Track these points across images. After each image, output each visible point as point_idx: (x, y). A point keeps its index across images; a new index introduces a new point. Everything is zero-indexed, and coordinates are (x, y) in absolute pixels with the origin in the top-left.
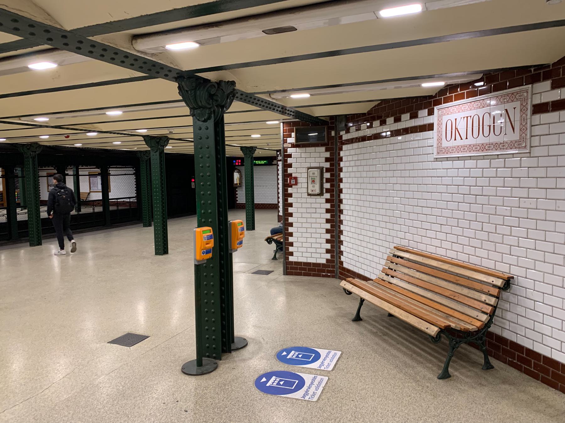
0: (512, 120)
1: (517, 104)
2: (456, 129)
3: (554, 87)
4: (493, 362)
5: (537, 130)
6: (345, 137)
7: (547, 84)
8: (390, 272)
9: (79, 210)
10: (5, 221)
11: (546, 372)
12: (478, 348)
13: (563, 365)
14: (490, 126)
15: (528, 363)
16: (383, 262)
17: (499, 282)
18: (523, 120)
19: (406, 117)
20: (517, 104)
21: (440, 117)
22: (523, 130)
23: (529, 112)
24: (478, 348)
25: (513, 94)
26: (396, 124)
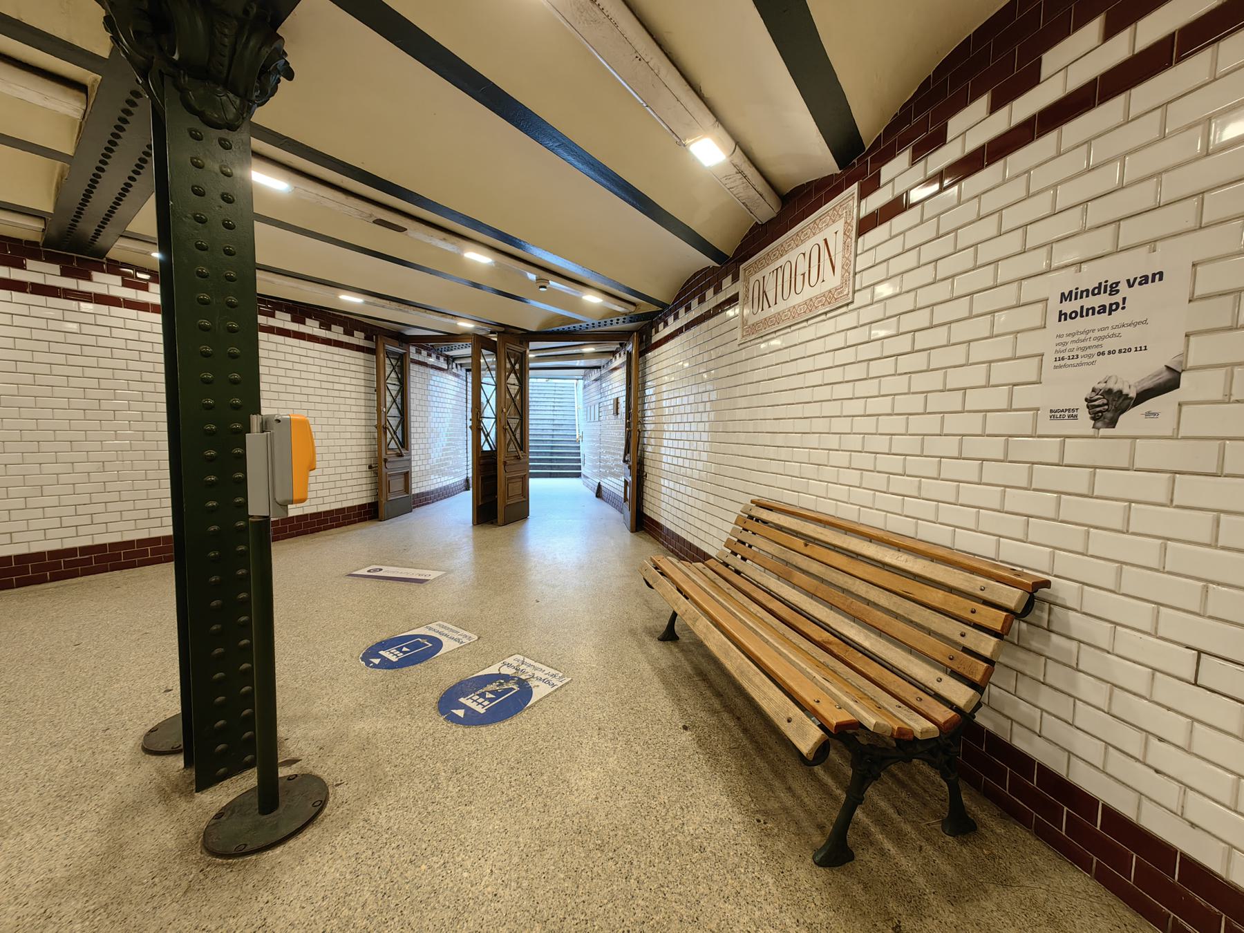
5: (862, 262)
6: (656, 338)
25: (797, 234)
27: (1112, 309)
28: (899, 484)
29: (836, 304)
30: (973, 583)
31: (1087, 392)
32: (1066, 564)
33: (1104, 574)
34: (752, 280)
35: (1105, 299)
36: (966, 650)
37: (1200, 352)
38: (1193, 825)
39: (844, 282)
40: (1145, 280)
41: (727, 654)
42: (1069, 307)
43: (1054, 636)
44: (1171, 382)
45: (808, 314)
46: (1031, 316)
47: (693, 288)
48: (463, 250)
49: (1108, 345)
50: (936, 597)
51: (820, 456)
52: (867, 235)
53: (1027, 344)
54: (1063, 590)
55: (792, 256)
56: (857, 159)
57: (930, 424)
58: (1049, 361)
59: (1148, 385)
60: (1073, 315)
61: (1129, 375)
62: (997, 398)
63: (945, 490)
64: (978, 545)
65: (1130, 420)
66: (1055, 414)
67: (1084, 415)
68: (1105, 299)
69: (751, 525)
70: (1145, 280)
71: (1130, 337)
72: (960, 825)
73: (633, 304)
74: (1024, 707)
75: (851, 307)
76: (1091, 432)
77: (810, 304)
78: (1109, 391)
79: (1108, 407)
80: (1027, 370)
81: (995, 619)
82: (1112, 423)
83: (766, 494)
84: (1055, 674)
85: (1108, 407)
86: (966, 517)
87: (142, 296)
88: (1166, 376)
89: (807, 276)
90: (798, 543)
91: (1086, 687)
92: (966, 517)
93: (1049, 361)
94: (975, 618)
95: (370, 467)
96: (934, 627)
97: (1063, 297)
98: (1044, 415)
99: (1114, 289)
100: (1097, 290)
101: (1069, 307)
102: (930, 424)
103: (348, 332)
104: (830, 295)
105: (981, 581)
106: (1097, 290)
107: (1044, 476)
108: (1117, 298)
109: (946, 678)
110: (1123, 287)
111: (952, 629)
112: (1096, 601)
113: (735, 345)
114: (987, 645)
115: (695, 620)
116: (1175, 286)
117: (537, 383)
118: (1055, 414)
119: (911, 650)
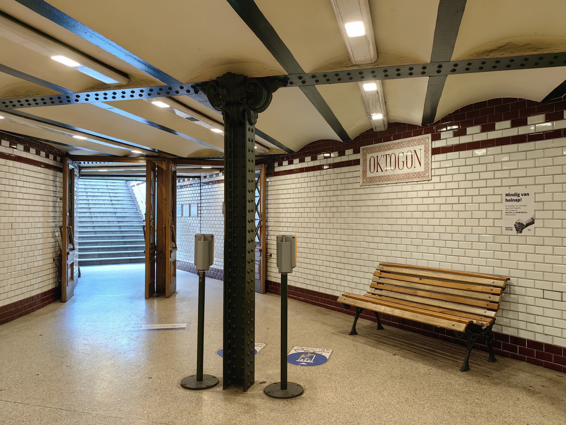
0: (419, 157)
1: (422, 147)
2: (378, 163)
3: (483, 131)
4: (497, 357)
5: (434, 165)
6: (277, 169)
7: (542, 117)
8: (380, 286)
9: (171, 111)
10: (374, 114)
11: (531, 353)
12: (481, 345)
13: (564, 349)
14: (403, 162)
15: (531, 353)
16: (371, 276)
17: (501, 283)
18: (426, 157)
19: (296, 161)
20: (422, 147)
21: (365, 155)
22: (426, 164)
23: (430, 152)
24: (481, 345)
25: (398, 143)
26: (340, 158)
27: (518, 201)
28: (456, 252)
29: (422, 178)
30: (490, 282)
31: (514, 223)
32: (513, 273)
33: (521, 274)
34: (369, 156)
35: (516, 198)
36: (491, 302)
37: (538, 215)
38: (546, 335)
39: (426, 170)
40: (525, 195)
41: (417, 317)
42: (508, 198)
43: (512, 295)
44: (532, 222)
45: (408, 179)
46: (498, 199)
47: (313, 148)
48: (151, 101)
49: (518, 210)
50: (480, 288)
51: (418, 242)
52: (436, 155)
53: (497, 207)
54: (513, 281)
55: (397, 151)
56: (430, 125)
57: (468, 230)
58: (504, 212)
59: (528, 222)
60: (509, 201)
61: (524, 219)
62: (490, 222)
63: (475, 253)
64: (488, 271)
65: (525, 231)
66: (507, 229)
67: (514, 229)
68: (516, 198)
69: (384, 275)
70: (525, 195)
71: (523, 209)
72: (493, 360)
73: (268, 148)
74: (505, 320)
75: (430, 182)
76: (516, 234)
77: (408, 176)
78: (520, 223)
79: (520, 227)
80: (498, 215)
81: (498, 290)
82: (521, 232)
83: (384, 260)
84: (513, 306)
85: (520, 227)
86: (482, 262)
87: (216, 178)
88: (531, 220)
89: (405, 163)
90: (417, 280)
91: (521, 308)
92: (482, 262)
93: (504, 212)
94: (492, 292)
95: (54, 260)
96: (480, 298)
97: (507, 195)
98: (504, 229)
99: (518, 195)
100: (515, 195)
101: (508, 198)
102: (468, 230)
103: (27, 150)
104: (418, 175)
105: (492, 281)
106: (515, 195)
107: (505, 247)
108: (519, 198)
109: (487, 311)
110: (520, 195)
111: (486, 297)
112: (522, 282)
113: (358, 186)
114: (497, 298)
115: (393, 312)
116: (531, 197)
117: (80, 184)
118: (507, 229)
119: (472, 306)
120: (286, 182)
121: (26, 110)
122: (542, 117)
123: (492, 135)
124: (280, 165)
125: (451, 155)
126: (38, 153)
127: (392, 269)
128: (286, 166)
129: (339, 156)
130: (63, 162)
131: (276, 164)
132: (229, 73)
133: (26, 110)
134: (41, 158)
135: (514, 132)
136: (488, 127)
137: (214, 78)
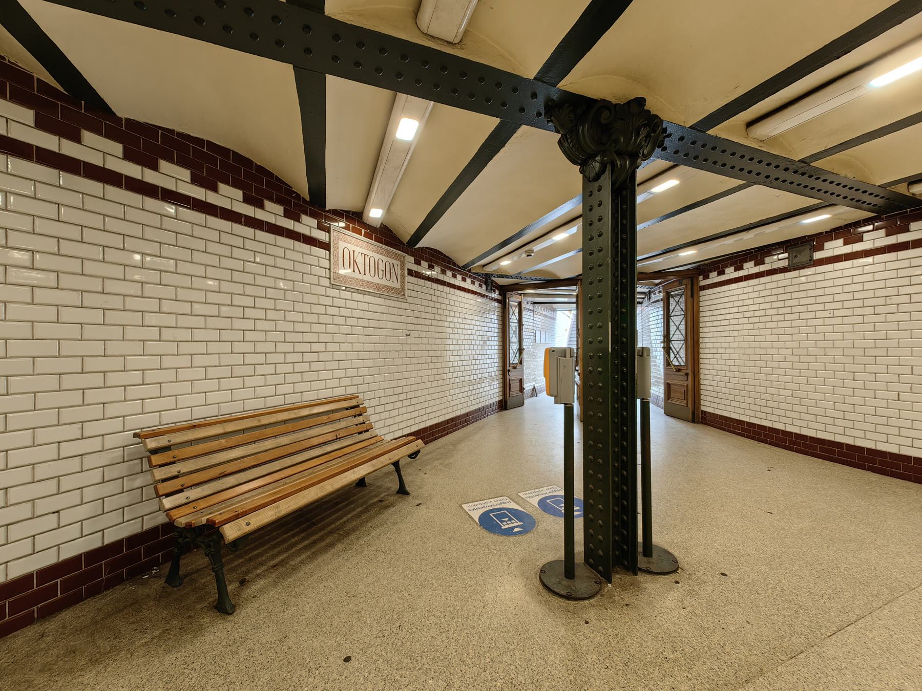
3: (735, 270)
6: (703, 283)
120: (727, 294)
121: (40, 72)
122: (882, 232)
123: (762, 268)
124: (706, 277)
125: (879, 258)
126: (464, 280)
127: (566, 300)
128: (714, 278)
129: (887, 236)
130: (504, 291)
131: (701, 278)
132: (544, 511)
133: (40, 72)
134: (475, 288)
135: (849, 249)
136: (739, 268)
137: (614, 101)
